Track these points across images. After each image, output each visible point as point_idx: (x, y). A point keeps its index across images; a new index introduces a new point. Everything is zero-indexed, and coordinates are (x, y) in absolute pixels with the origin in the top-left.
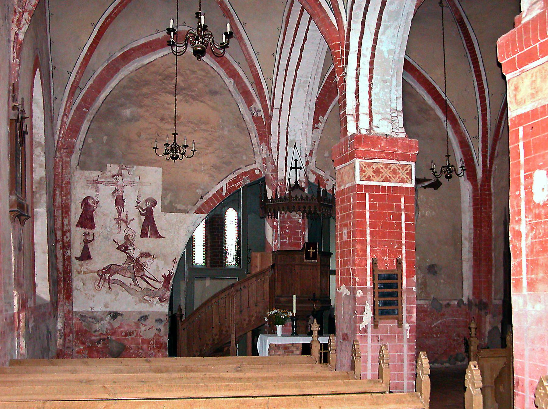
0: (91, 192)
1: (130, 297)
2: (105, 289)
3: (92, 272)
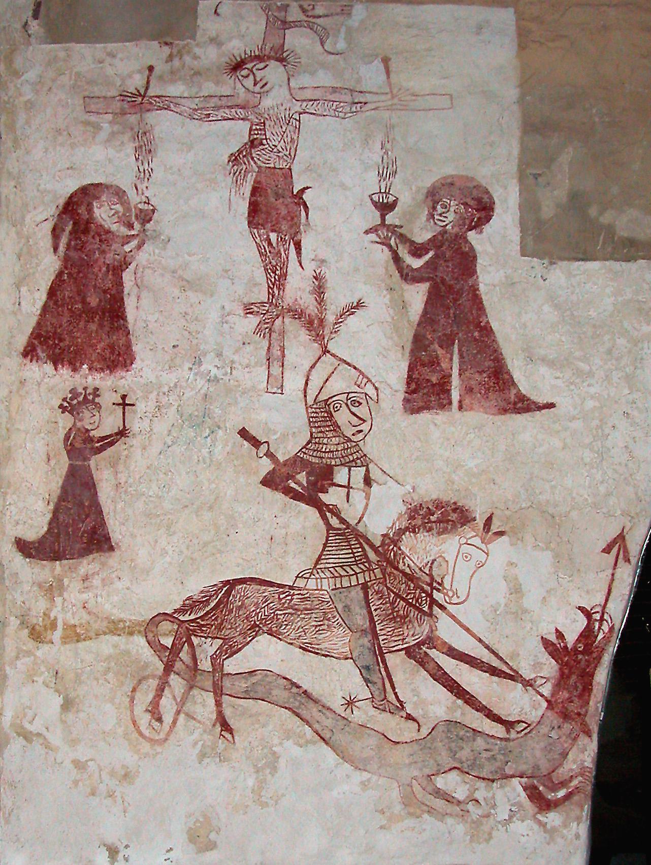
0: (103, 160)
1: (348, 783)
2: (192, 733)
3: (115, 627)
